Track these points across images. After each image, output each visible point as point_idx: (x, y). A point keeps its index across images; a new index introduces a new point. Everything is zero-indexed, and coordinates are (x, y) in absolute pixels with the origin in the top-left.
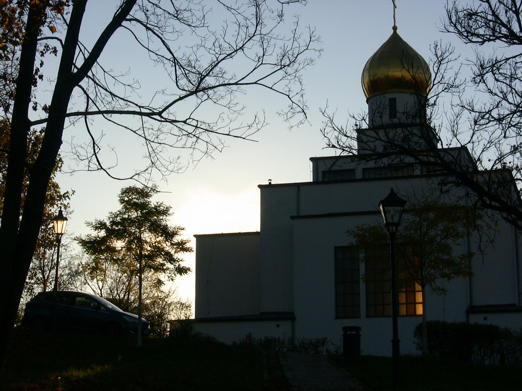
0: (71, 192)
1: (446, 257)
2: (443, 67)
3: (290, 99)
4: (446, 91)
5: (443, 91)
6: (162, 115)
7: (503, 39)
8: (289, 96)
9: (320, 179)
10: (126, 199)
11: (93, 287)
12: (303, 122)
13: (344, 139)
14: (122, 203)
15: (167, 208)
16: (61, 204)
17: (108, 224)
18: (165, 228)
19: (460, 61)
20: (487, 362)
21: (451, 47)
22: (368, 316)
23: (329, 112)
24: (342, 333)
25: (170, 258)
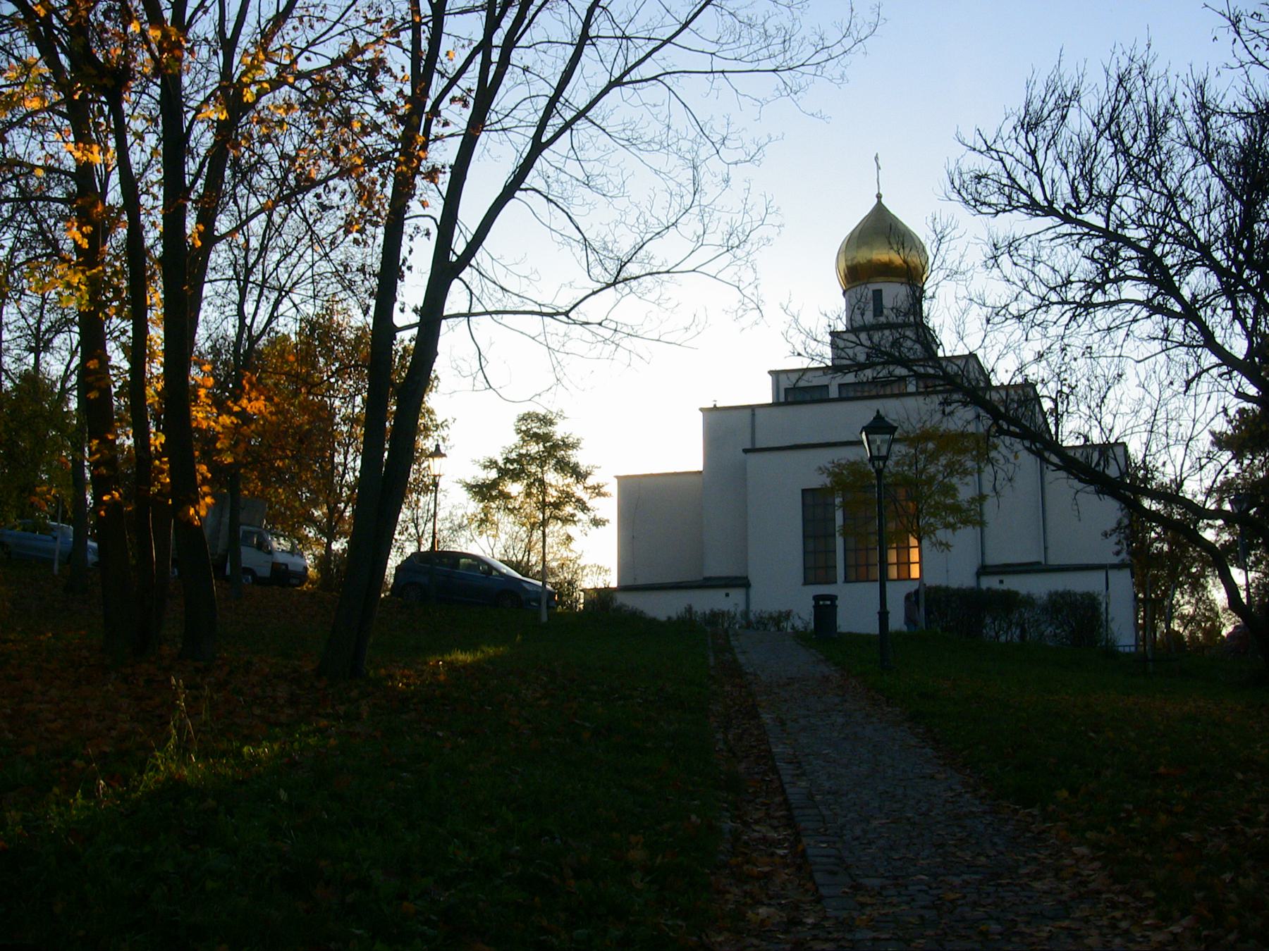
0: (450, 420)
7: (1022, 210)
9: (782, 399)
13: (813, 344)
20: (1003, 638)
22: (847, 580)
23: (793, 309)
24: (813, 603)
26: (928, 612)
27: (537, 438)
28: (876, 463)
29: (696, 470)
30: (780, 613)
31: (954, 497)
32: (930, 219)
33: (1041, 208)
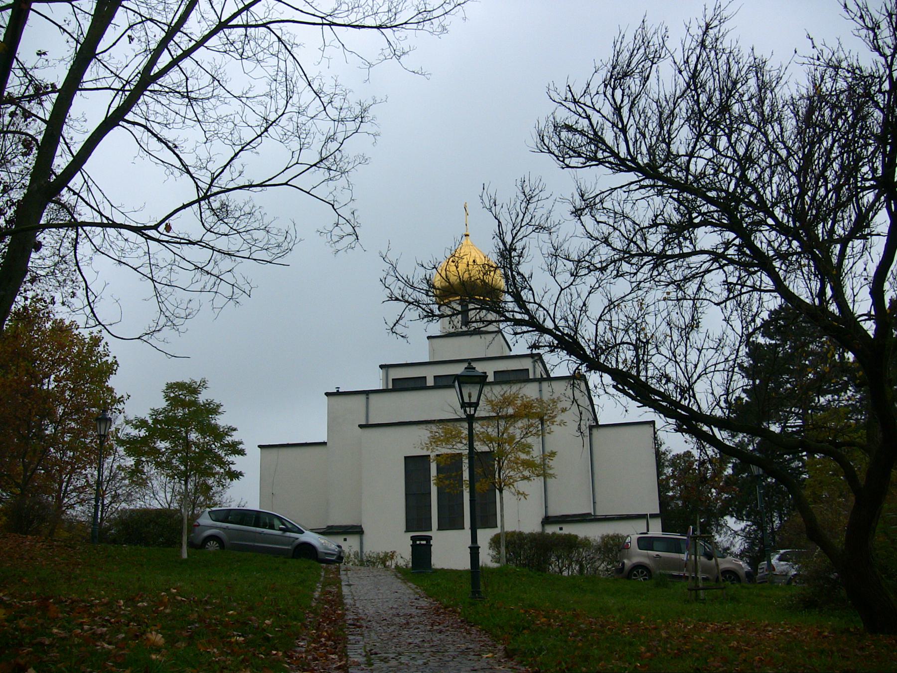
0: (126, 396)
1: (523, 456)
2: (531, 207)
3: (335, 210)
4: (538, 231)
5: (533, 231)
6: (159, 229)
7: (607, 165)
8: (333, 206)
9: (390, 387)
10: (172, 395)
11: (161, 502)
12: (353, 245)
13: (410, 291)
14: (167, 400)
15: (217, 406)
16: (116, 409)
17: (150, 422)
18: (216, 427)
19: (551, 200)
20: (565, 573)
21: (541, 183)
22: (440, 528)
23: (392, 257)
24: (411, 542)
25: (222, 463)
26: (507, 547)
27: (184, 404)
28: (468, 409)
29: (90, 160)
30: (386, 554)
31: (528, 453)
32: (519, 183)
33: (623, 161)
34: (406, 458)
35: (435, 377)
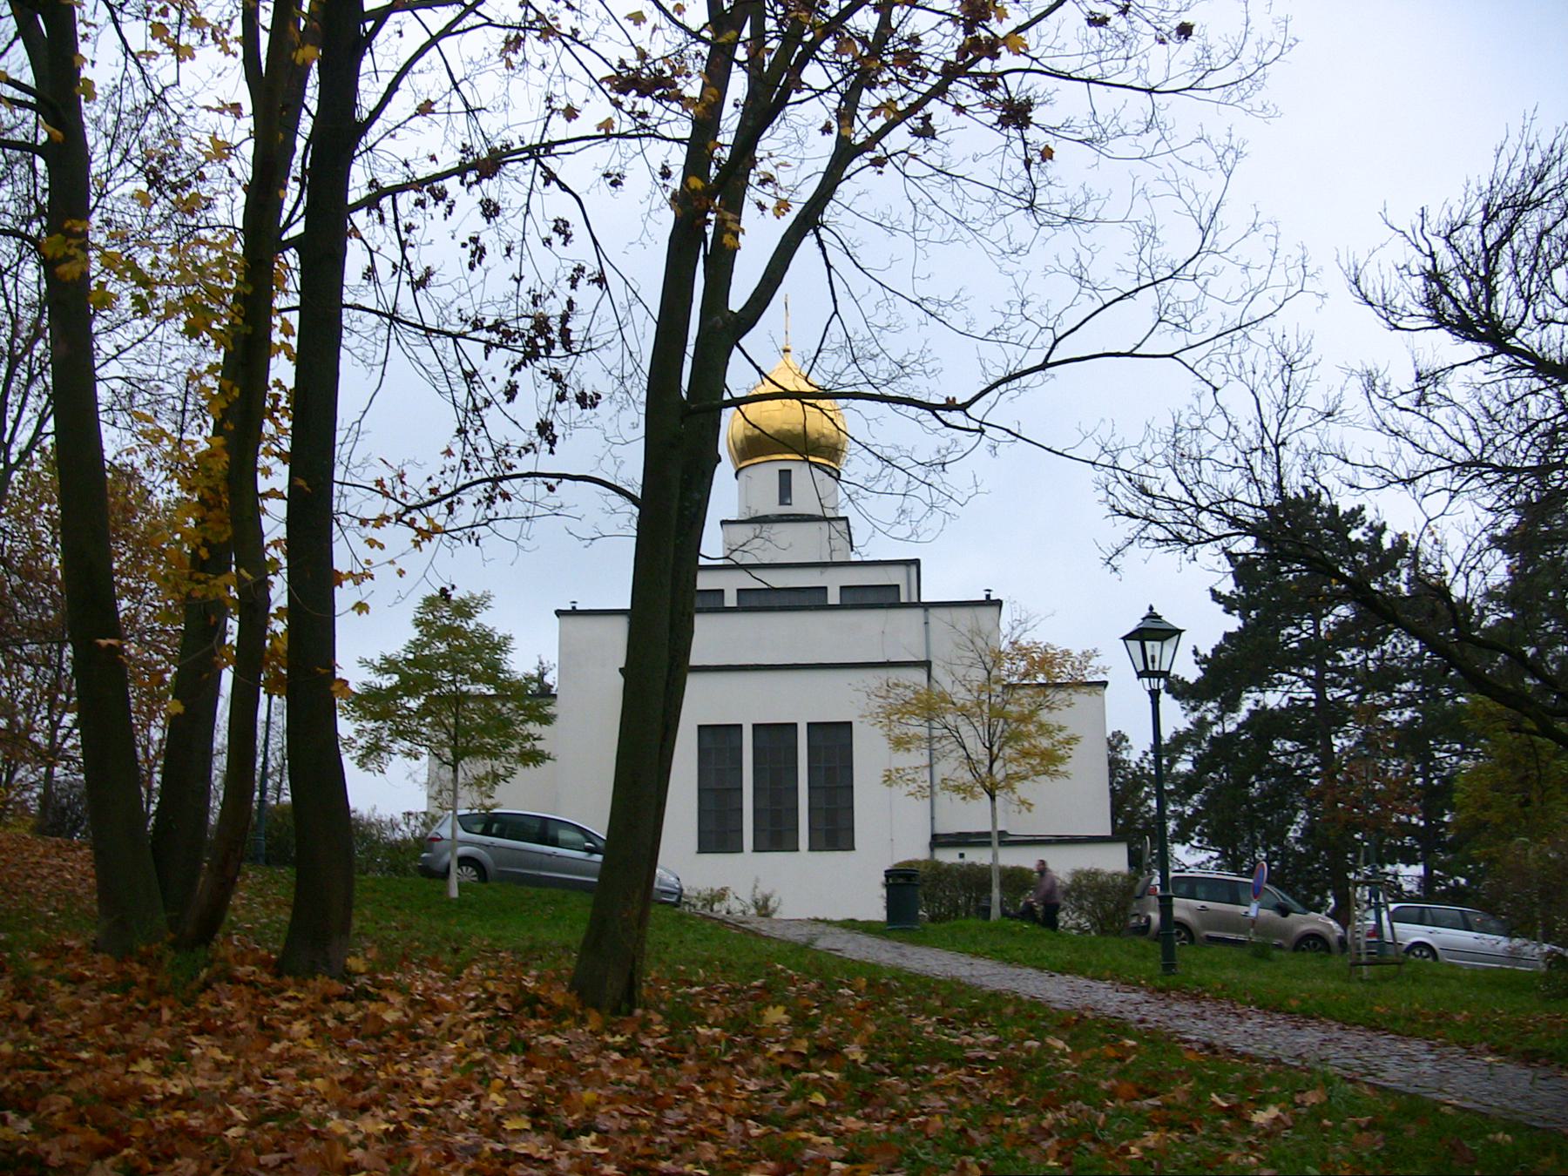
34: (700, 727)
35: (738, 590)
